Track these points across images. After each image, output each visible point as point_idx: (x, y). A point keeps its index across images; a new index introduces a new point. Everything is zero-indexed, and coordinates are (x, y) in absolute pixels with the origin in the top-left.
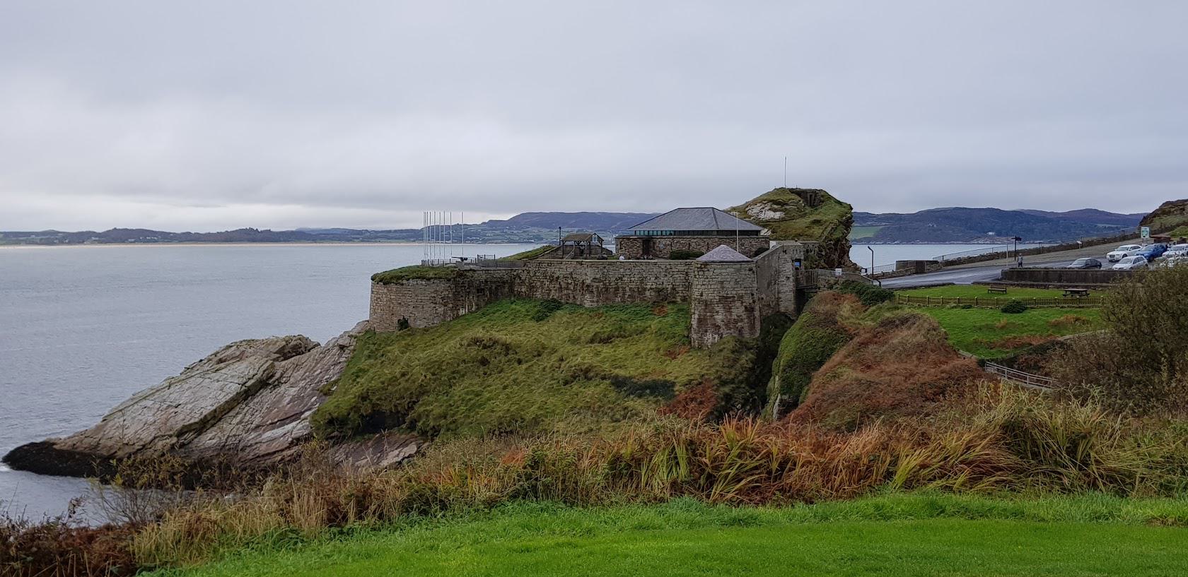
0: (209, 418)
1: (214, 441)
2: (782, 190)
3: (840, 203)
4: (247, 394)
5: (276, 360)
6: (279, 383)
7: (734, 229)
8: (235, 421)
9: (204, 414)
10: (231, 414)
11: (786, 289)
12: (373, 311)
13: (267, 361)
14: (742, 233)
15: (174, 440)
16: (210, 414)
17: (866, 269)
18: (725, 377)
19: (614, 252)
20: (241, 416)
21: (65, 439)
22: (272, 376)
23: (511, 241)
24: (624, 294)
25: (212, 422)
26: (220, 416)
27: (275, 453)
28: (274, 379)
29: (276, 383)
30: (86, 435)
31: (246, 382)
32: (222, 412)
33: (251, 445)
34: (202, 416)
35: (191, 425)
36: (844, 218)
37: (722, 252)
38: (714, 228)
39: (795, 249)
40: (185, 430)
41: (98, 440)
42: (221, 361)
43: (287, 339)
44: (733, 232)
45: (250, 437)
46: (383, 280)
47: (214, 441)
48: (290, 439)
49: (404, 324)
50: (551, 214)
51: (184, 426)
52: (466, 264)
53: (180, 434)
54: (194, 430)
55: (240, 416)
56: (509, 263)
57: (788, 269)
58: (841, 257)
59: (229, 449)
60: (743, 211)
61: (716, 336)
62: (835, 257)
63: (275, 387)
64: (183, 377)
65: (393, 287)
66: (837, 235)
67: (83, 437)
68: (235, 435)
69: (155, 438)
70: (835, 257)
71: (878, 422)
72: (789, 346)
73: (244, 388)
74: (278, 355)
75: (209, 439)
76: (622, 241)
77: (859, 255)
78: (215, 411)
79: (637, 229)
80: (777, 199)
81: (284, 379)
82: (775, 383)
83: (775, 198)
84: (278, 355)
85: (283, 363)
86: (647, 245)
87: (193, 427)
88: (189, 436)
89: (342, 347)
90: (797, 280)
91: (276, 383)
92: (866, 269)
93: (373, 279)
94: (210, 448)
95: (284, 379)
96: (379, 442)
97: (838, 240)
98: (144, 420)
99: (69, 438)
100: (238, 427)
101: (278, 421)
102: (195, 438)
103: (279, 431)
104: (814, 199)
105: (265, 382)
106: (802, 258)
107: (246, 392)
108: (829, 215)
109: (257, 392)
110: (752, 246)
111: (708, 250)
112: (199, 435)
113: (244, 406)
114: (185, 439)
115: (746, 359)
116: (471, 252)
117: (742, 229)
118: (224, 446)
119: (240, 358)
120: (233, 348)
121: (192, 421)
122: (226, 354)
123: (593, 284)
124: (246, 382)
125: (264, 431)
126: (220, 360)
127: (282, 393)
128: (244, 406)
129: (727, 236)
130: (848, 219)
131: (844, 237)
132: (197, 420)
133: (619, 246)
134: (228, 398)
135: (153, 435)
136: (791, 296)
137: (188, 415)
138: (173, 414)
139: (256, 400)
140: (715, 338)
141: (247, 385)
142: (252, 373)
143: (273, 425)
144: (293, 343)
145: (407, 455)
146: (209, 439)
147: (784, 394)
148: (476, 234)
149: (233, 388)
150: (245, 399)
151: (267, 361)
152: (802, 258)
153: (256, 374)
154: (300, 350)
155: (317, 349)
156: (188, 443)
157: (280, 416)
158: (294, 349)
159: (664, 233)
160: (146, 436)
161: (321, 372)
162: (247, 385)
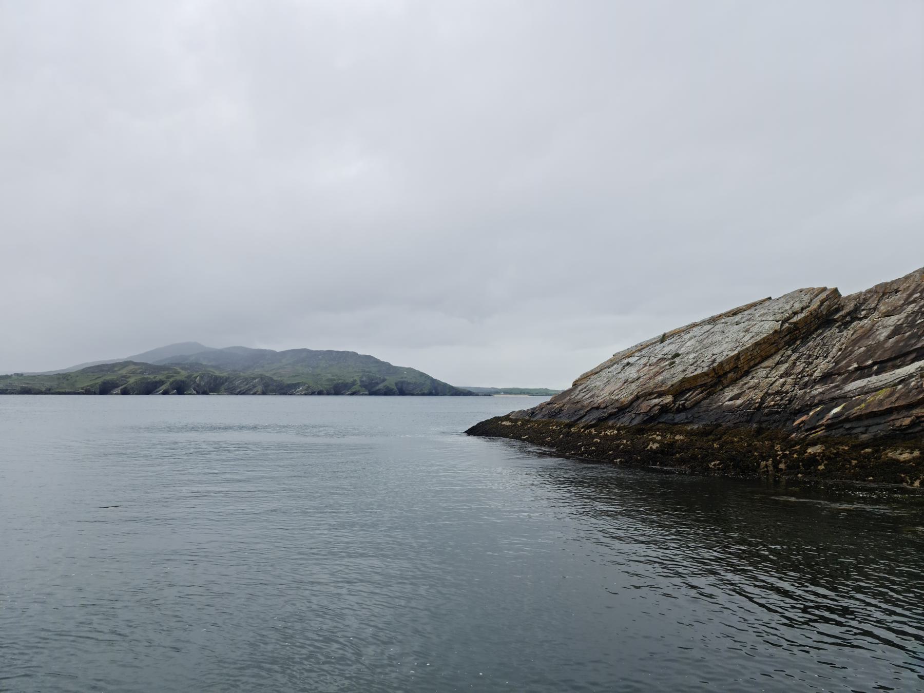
0: (727, 368)
9: (718, 361)
15: (668, 399)
16: (728, 361)
18: (836, 441)
20: (786, 365)
26: (746, 369)
32: (750, 360)
35: (697, 377)
40: (687, 385)
41: (561, 405)
51: (684, 380)
54: (701, 386)
59: (770, 414)
71: (901, 449)
78: (737, 357)
81: (863, 313)
87: (700, 382)
88: (693, 396)
91: (848, 319)
95: (863, 313)
98: (624, 379)
100: (782, 380)
102: (704, 398)
107: (789, 331)
109: (813, 333)
112: (710, 394)
113: (789, 352)
114: (686, 400)
121: (699, 371)
125: (845, 381)
128: (789, 352)
137: (691, 365)
141: (791, 321)
143: (863, 371)
147: (649, 463)
156: (692, 407)
157: (877, 356)
160: (625, 396)
162: (791, 321)
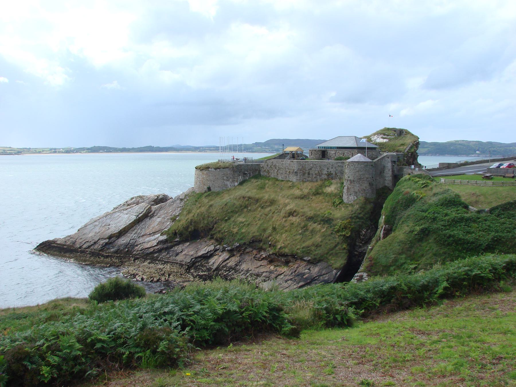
1: (125, 241)
2: (388, 129)
3: (413, 135)
4: (139, 221)
5: (153, 205)
6: (152, 216)
7: (365, 146)
8: (134, 233)
10: (132, 229)
11: (389, 175)
12: (196, 183)
13: (148, 205)
14: (368, 148)
15: (107, 240)
17: (425, 167)
19: (309, 156)
20: (136, 230)
21: (62, 239)
22: (150, 212)
23: (266, 152)
24: (312, 176)
25: (124, 233)
27: (150, 247)
28: (151, 214)
29: (152, 216)
30: (71, 237)
31: (138, 215)
33: (140, 244)
34: (119, 230)
36: (415, 142)
37: (358, 157)
38: (356, 146)
39: (393, 156)
41: (76, 239)
42: (128, 205)
43: (158, 195)
44: (364, 148)
45: (140, 240)
46: (200, 169)
47: (125, 241)
48: (157, 242)
49: (209, 189)
50: (283, 139)
52: (239, 161)
53: (110, 237)
55: (136, 230)
56: (261, 161)
57: (389, 165)
58: (413, 161)
60: (369, 139)
61: (355, 197)
62: (411, 160)
63: (151, 217)
64: (112, 212)
65: (205, 172)
66: (413, 150)
67: (69, 238)
68: (133, 239)
69: (99, 239)
70: (411, 160)
72: (388, 205)
73: (138, 218)
74: (153, 203)
75: (123, 241)
76: (312, 152)
77: (421, 160)
79: (320, 145)
80: (385, 132)
82: (382, 219)
83: (384, 132)
84: (153, 203)
85: (155, 206)
86: (323, 153)
89: (181, 200)
90: (393, 171)
91: (152, 216)
92: (425, 167)
93: (196, 168)
94: (122, 244)
96: (110, 283)
97: (412, 153)
99: (64, 238)
101: (152, 233)
102: (117, 240)
103: (153, 238)
104: (401, 133)
105: (147, 215)
106: (396, 161)
108: (409, 141)
110: (373, 155)
111: (352, 156)
112: (118, 238)
115: (369, 207)
116: (241, 156)
117: (369, 147)
118: (128, 244)
119: (138, 203)
120: (135, 199)
122: (131, 202)
123: (298, 171)
124: (138, 215)
126: (128, 204)
127: (154, 220)
129: (361, 149)
130: (417, 144)
131: (415, 151)
132: (117, 232)
133: (311, 154)
134: (130, 222)
135: (99, 238)
136: (390, 178)
138: (108, 229)
139: (143, 223)
140: (355, 198)
142: (141, 211)
144: (161, 197)
145: (209, 250)
146: (123, 241)
148: (250, 148)
149: (133, 218)
150: (138, 223)
151: (148, 205)
152: (396, 161)
153: (143, 211)
154: (163, 201)
155: (171, 200)
158: (161, 200)
159: (332, 148)
161: (172, 211)
